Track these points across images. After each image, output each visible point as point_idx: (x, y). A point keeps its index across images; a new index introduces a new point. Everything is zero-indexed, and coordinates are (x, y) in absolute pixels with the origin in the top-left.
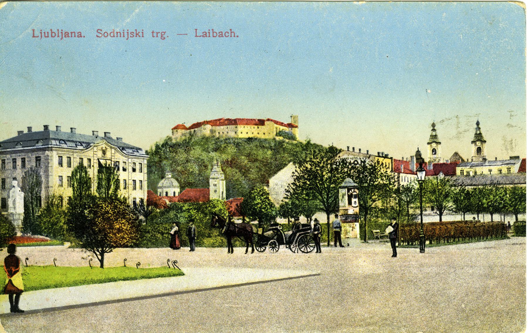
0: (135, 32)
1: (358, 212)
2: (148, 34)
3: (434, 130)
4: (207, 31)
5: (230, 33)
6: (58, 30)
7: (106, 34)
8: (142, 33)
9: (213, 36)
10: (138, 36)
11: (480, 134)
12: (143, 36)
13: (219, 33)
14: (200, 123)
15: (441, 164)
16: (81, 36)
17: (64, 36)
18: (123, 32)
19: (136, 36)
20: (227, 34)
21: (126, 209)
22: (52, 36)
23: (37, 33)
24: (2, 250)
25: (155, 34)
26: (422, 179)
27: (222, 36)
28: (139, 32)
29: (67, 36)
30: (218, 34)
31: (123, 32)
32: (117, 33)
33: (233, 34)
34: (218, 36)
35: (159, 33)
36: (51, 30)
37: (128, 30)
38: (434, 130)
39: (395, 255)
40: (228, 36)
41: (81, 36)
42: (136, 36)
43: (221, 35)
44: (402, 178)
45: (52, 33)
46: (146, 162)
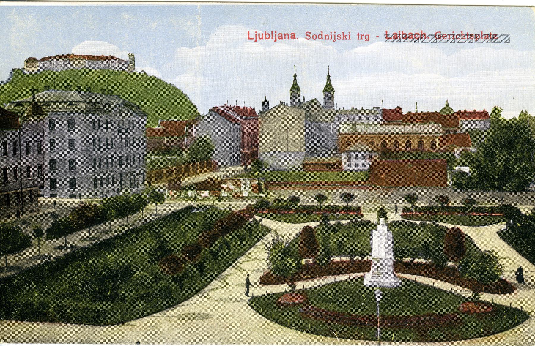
0: (342, 35)
2: (354, 36)
4: (329, 34)
6: (272, 32)
7: (315, 37)
8: (349, 35)
9: (266, 38)
10: (345, 38)
11: (297, 84)
12: (349, 39)
13: (494, 35)
14: (73, 56)
17: (277, 38)
18: (331, 35)
19: (343, 39)
24: (1, 323)
25: (360, 37)
28: (346, 35)
29: (280, 37)
31: (331, 35)
32: (326, 36)
35: (364, 35)
36: (265, 32)
37: (335, 33)
39: (511, 303)
41: (295, 38)
42: (343, 39)
45: (266, 34)
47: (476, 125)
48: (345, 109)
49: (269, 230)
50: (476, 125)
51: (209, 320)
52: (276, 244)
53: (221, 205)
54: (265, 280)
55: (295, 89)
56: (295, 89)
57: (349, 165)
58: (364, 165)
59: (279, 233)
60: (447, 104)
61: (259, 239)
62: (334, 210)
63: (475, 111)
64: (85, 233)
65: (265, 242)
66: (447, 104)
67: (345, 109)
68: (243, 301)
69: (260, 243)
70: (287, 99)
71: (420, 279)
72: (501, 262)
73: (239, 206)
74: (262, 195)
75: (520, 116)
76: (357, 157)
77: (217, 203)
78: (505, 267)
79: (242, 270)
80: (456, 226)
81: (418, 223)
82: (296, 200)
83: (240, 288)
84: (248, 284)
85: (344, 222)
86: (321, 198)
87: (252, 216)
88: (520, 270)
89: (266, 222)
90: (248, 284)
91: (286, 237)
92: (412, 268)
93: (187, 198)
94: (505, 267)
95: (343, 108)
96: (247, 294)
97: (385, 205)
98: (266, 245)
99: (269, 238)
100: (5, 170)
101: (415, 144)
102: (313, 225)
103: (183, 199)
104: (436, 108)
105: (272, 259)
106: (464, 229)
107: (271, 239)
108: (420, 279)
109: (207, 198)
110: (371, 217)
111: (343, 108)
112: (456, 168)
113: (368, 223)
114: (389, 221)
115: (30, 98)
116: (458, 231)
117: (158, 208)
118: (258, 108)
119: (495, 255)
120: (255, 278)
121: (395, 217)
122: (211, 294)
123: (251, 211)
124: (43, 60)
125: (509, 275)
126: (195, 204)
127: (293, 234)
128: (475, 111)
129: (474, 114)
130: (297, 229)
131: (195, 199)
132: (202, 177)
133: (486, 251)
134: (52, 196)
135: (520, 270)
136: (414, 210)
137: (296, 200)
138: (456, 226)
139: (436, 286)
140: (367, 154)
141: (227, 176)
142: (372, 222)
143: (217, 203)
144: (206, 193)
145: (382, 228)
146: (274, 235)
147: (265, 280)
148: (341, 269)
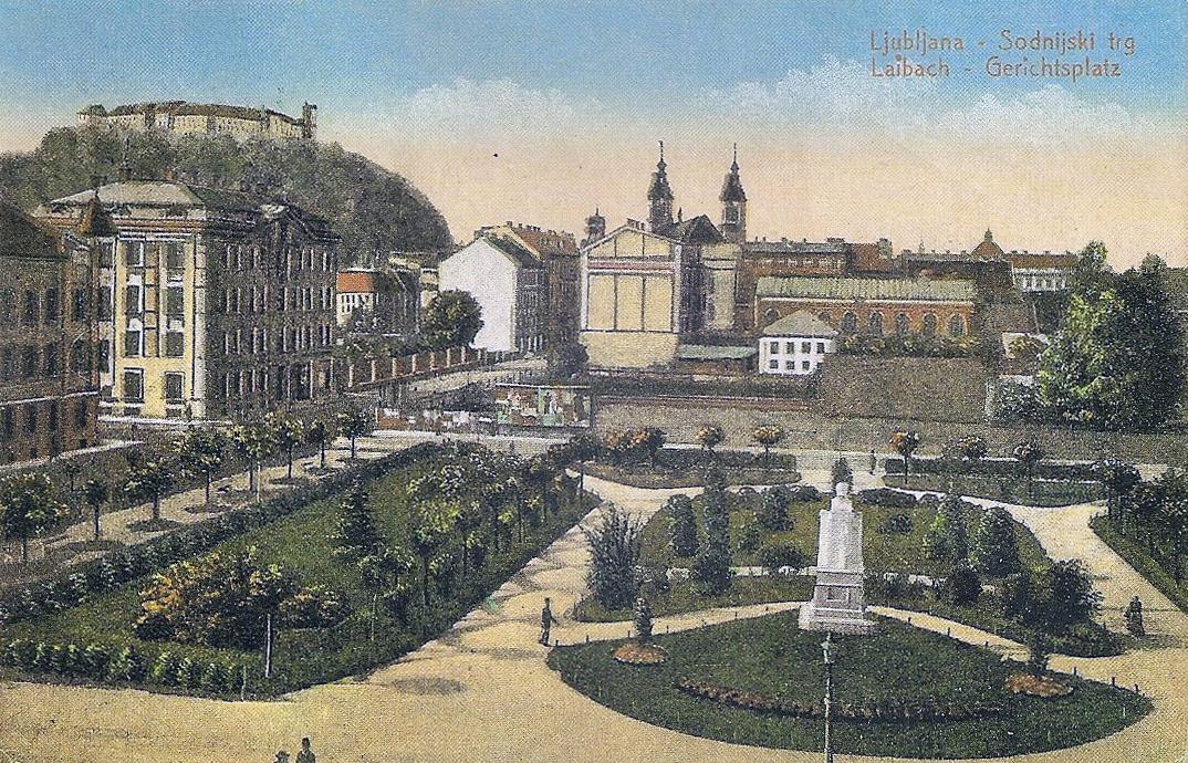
47: (1049, 285)
48: (767, 240)
49: (592, 502)
50: (1049, 285)
51: (457, 697)
52: (614, 529)
53: (496, 442)
54: (580, 615)
55: (660, 191)
56: (660, 191)
57: (774, 364)
58: (806, 365)
59: (619, 509)
60: (988, 235)
61: (574, 521)
62: (739, 461)
63: (988, 243)
64: (197, 496)
65: (587, 528)
66: (988, 235)
67: (767, 240)
68: (531, 654)
69: (575, 529)
70: (643, 212)
71: (922, 621)
72: (1096, 586)
73: (531, 446)
74: (584, 424)
75: (1143, 268)
76: (791, 348)
77: (486, 439)
78: (1102, 599)
79: (537, 588)
80: (1001, 505)
81: (919, 495)
82: (656, 438)
83: (527, 626)
84: (547, 619)
85: (759, 489)
86: (715, 437)
87: (562, 467)
88: (1136, 607)
89: (590, 483)
90: (547, 619)
91: (632, 517)
92: (896, 594)
93: (419, 426)
94: (1102, 599)
95: (764, 239)
96: (544, 641)
97: (850, 455)
98: (588, 533)
99: (595, 519)
100: (7, 352)
101: (915, 326)
102: (692, 493)
103: (414, 428)
104: (959, 241)
105: (600, 561)
106: (1018, 512)
107: (600, 522)
108: (922, 621)
109: (466, 428)
110: (817, 478)
111: (764, 239)
112: (1006, 378)
113: (811, 496)
114: (856, 490)
115: (88, 195)
116: (1005, 516)
117: (359, 445)
118: (580, 235)
119: (1081, 572)
120: (561, 607)
121: (868, 480)
122: (467, 638)
123: (560, 457)
124: (119, 111)
125: (1110, 618)
126: (438, 440)
127: (647, 513)
128: (988, 243)
129: (1044, 260)
130: (656, 501)
131: (439, 430)
132: (452, 382)
133: (1062, 562)
134: (128, 412)
135: (1136, 607)
136: (910, 467)
137: (656, 438)
138: (1001, 505)
139: (954, 635)
140: (814, 342)
141: (510, 380)
142: (820, 491)
143: (486, 439)
144: (463, 417)
145: (841, 505)
146: (606, 511)
147: (580, 615)
148: (759, 593)
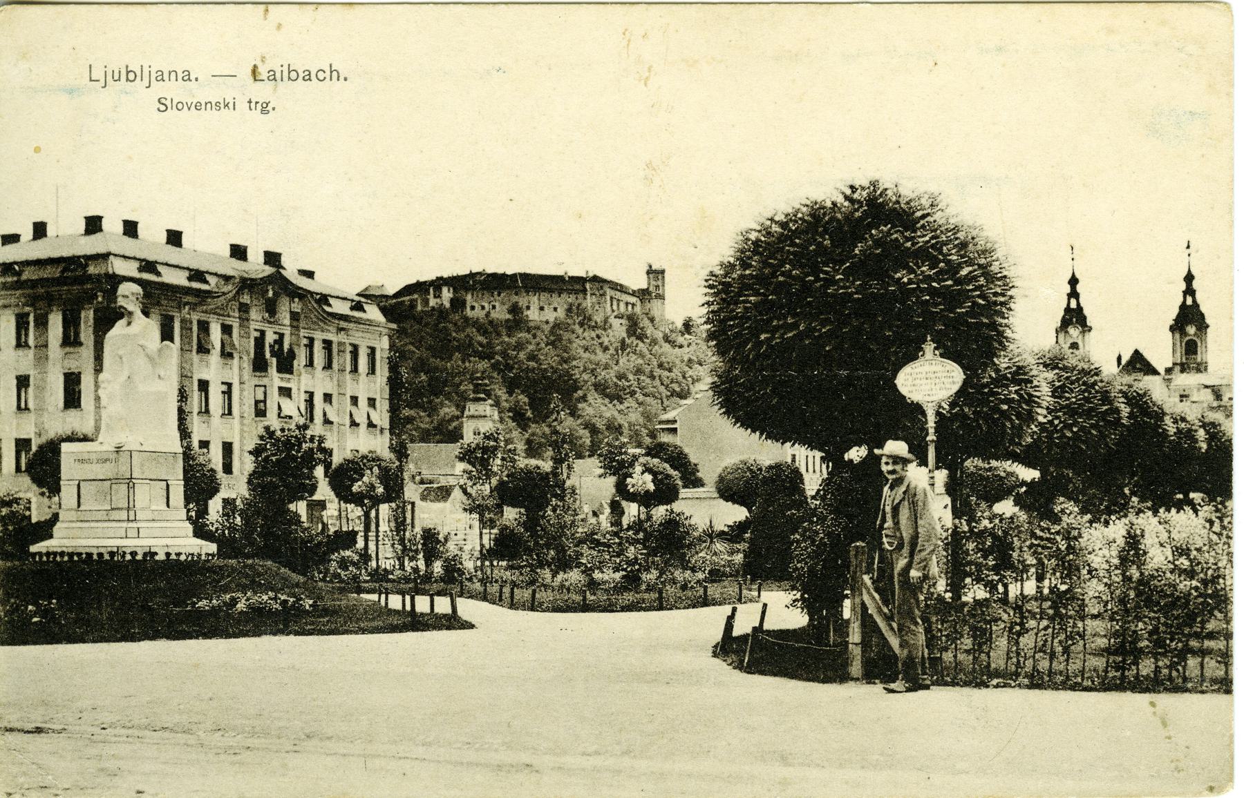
1: (748, 515)
3: (1074, 294)
5: (328, 72)
11: (1196, 305)
15: (819, 451)
16: (189, 79)
20: (321, 75)
21: (267, 457)
22: (127, 80)
23: (263, 71)
26: (428, 598)
27: (310, 79)
30: (301, 75)
33: (335, 74)
34: (301, 78)
38: (1074, 294)
40: (325, 78)
43: (308, 77)
44: (1181, 345)
45: (128, 72)
46: (385, 343)
